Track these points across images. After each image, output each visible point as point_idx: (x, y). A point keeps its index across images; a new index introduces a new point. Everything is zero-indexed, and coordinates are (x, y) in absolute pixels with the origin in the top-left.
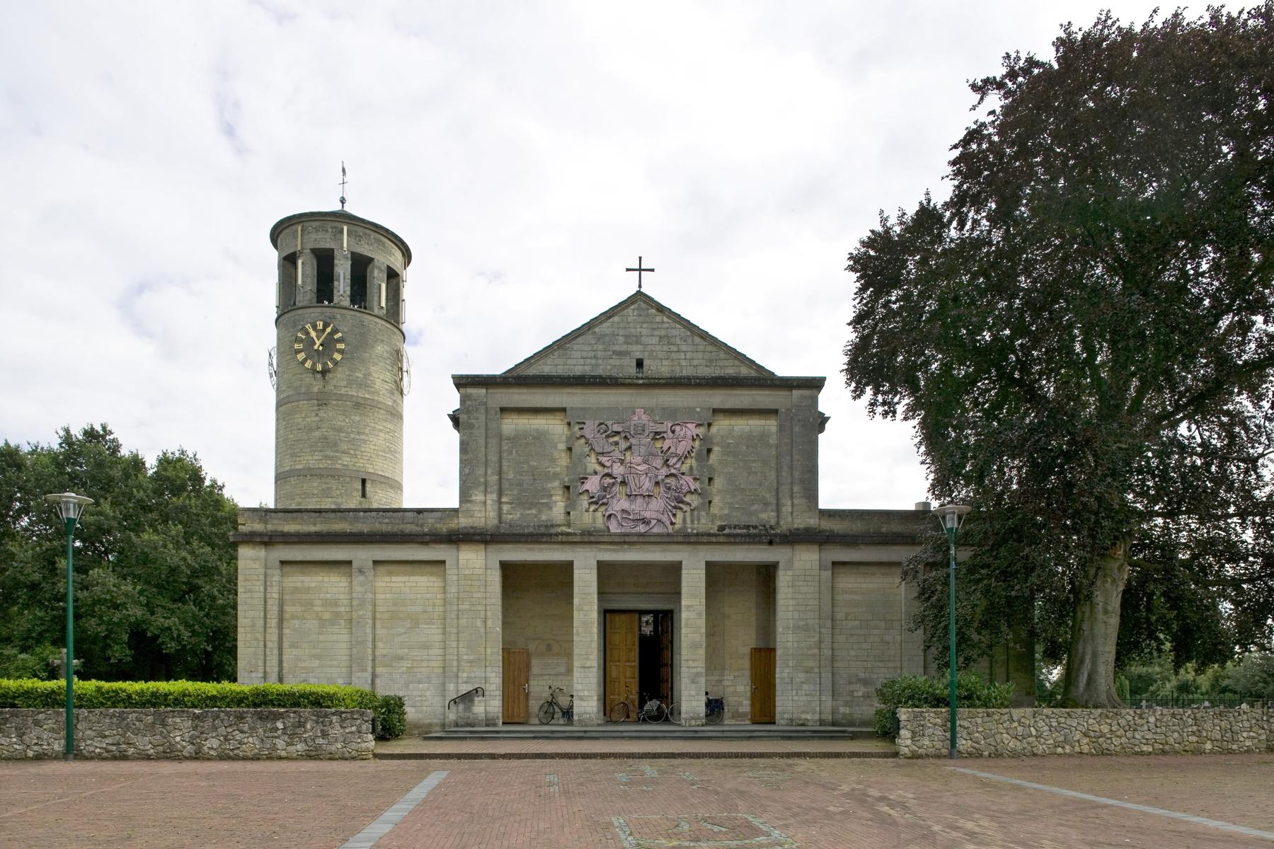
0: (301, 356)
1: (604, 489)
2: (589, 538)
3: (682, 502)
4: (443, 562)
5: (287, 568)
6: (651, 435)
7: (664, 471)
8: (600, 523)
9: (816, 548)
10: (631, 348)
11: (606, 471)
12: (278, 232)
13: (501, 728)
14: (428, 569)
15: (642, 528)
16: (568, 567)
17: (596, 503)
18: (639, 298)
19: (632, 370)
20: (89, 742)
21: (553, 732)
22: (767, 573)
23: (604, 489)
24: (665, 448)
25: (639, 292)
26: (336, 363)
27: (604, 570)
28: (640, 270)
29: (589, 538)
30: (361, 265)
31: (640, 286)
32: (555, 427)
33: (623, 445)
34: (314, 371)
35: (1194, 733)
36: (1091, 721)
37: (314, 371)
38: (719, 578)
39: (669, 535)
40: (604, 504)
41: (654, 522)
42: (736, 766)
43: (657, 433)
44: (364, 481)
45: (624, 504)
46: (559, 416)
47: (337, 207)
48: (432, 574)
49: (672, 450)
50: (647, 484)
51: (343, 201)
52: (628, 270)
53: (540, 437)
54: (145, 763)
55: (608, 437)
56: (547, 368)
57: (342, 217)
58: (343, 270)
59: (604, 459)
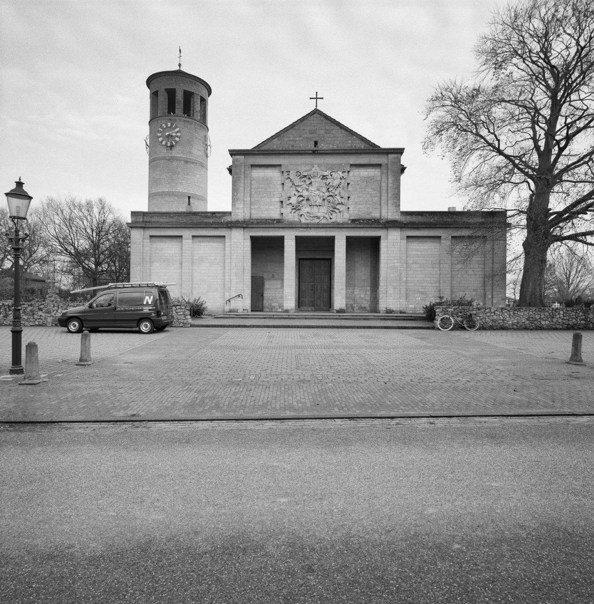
0: (160, 139)
2: (292, 226)
3: (335, 208)
4: (224, 236)
5: (196, 239)
7: (327, 194)
8: (296, 219)
9: (399, 230)
12: (150, 81)
15: (317, 221)
16: (332, 239)
18: (316, 112)
19: (311, 146)
21: (297, 315)
22: (375, 243)
24: (328, 183)
26: (176, 142)
27: (299, 239)
28: (317, 98)
29: (292, 226)
30: (188, 96)
31: (316, 106)
33: (308, 182)
35: (583, 320)
37: (166, 145)
38: (351, 243)
40: (299, 209)
41: (322, 218)
43: (324, 176)
44: (189, 198)
45: (308, 209)
47: (177, 68)
50: (319, 201)
51: (180, 65)
53: (267, 181)
57: (179, 74)
58: (179, 97)
59: (299, 189)
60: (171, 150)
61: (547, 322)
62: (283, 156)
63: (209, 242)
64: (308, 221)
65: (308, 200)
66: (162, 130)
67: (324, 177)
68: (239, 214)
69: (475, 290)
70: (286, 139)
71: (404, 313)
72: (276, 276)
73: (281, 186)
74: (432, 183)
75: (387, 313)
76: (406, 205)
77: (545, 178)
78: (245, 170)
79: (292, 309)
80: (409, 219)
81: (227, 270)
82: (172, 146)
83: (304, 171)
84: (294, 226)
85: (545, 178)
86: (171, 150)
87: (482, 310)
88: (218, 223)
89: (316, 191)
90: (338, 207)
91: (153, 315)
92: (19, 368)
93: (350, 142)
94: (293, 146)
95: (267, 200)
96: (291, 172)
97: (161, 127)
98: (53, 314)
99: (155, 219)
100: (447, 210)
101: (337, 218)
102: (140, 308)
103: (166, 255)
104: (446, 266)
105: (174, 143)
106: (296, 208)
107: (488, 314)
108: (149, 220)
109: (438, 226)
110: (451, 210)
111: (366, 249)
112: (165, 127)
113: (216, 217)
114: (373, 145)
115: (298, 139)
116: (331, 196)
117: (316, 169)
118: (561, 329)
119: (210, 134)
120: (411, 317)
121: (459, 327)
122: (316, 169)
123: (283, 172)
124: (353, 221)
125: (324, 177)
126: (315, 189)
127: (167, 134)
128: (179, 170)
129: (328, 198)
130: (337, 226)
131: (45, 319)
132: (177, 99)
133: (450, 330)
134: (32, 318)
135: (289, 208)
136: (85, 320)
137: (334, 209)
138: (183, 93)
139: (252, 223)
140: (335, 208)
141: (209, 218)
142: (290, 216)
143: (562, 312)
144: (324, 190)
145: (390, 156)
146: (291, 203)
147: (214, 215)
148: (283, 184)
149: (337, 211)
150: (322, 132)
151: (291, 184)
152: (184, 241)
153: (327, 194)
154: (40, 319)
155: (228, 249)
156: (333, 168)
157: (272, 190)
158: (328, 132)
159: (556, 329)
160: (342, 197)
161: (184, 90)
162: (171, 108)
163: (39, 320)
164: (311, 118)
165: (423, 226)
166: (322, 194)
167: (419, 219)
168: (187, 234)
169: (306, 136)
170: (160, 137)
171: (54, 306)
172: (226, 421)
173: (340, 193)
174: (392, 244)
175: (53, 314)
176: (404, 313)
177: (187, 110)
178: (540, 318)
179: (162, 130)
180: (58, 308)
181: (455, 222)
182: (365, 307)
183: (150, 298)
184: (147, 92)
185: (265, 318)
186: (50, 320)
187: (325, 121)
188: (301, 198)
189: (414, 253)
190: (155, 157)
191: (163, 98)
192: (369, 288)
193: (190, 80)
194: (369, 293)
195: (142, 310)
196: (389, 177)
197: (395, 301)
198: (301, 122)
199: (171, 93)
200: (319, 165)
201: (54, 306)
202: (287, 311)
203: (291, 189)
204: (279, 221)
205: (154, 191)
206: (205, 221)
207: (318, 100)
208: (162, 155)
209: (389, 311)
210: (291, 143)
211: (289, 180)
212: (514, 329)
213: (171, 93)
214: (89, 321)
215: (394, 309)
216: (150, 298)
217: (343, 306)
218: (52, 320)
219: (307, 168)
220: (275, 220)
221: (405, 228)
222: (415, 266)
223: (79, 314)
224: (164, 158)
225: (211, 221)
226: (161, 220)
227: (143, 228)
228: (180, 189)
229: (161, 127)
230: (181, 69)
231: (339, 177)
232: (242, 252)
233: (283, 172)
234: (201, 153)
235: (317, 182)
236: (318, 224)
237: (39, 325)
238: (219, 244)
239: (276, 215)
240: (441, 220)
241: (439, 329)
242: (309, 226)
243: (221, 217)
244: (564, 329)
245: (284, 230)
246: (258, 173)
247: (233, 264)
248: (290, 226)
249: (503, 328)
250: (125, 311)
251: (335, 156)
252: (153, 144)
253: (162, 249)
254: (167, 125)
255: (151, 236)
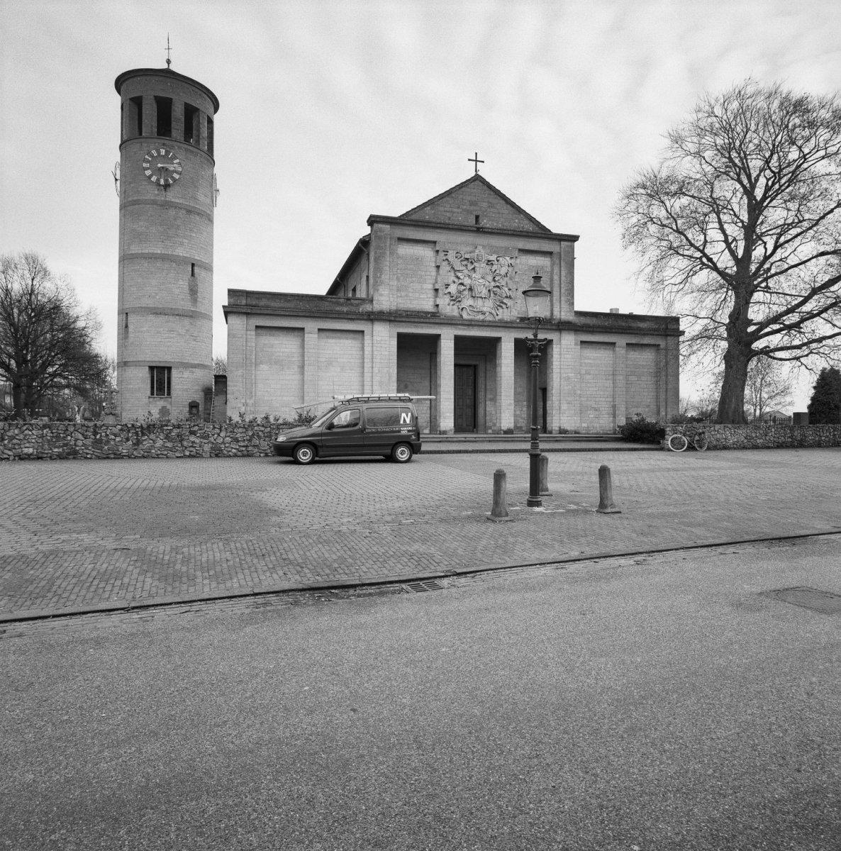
0: (148, 173)
1: (460, 292)
2: (450, 322)
3: (503, 303)
4: (363, 332)
5: (323, 334)
6: (486, 262)
7: (493, 284)
8: (456, 313)
9: (573, 333)
10: (472, 208)
11: (460, 281)
13: (451, 434)
14: (352, 335)
15: (481, 317)
16: (437, 338)
17: (454, 300)
18: (478, 178)
19: (472, 221)
20: (227, 445)
21: (525, 437)
23: (460, 292)
24: (493, 270)
25: (477, 175)
26: (175, 180)
27: (459, 340)
29: (450, 322)
30: (191, 112)
32: (426, 252)
33: (470, 267)
34: (158, 184)
35: (790, 437)
36: (748, 431)
37: (158, 184)
38: (520, 345)
39: (495, 322)
40: (460, 301)
41: (488, 313)
42: (431, 460)
43: (489, 261)
44: (193, 265)
45: (470, 302)
46: (432, 245)
47: (165, 66)
48: (354, 339)
49: (497, 272)
50: (484, 292)
51: (169, 62)
52: (483, 162)
53: (418, 260)
54: (756, 452)
55: (462, 261)
56: (428, 215)
57: (167, 74)
58: (178, 112)
59: (459, 274)
60: (165, 190)
61: (761, 441)
62: (438, 231)
63: (340, 338)
64: (470, 317)
65: (471, 289)
66: (150, 159)
67: (489, 262)
68: (384, 302)
69: (648, 406)
70: (442, 209)
71: (578, 433)
72: (410, 387)
73: (434, 269)
74: (609, 279)
75: (560, 433)
76: (581, 304)
77: (743, 282)
78: (391, 244)
79: (451, 430)
80: (583, 320)
81: (368, 375)
82: (167, 186)
83: (464, 250)
84: (453, 322)
85: (743, 282)
86: (165, 190)
87: (708, 428)
88: (354, 313)
89: (480, 280)
90: (505, 301)
91: (413, 437)
92: (535, 500)
93: (517, 221)
94: (450, 218)
95: (417, 286)
96: (450, 252)
97: (149, 153)
98: (212, 439)
99: (263, 302)
100: (608, 312)
101: (504, 315)
102: (397, 429)
103: (278, 354)
104: (621, 378)
105: (171, 182)
106: (456, 299)
107: (713, 433)
108: (254, 303)
109: (614, 331)
110: (614, 312)
111: (533, 357)
112: (155, 155)
113: (352, 305)
114: (543, 228)
115: (455, 210)
116: (498, 287)
117: (480, 251)
118: (772, 448)
119: (216, 170)
120: (602, 437)
121: (691, 448)
122: (480, 251)
123: (437, 251)
124: (522, 319)
125: (489, 262)
126: (480, 276)
127: (159, 165)
128: (179, 222)
129: (495, 289)
130: (504, 325)
131: (200, 446)
132: (166, 116)
133: (684, 451)
134: (180, 445)
135: (447, 299)
136: (322, 447)
137: (501, 305)
138: (183, 108)
139: (400, 315)
140: (503, 303)
141: (342, 305)
142: (448, 309)
143: (773, 430)
144: (490, 278)
145: (564, 244)
146: (450, 293)
147: (349, 302)
148: (438, 267)
149: (504, 306)
150: (485, 205)
151: (448, 268)
152: (306, 335)
153: (493, 284)
154: (192, 446)
155: (368, 349)
156: (506, 252)
157: (423, 273)
158: (491, 205)
159: (768, 448)
160: (510, 289)
161: (156, 97)
162: (164, 128)
163: (192, 449)
164: (471, 185)
165: (598, 330)
166: (487, 284)
167: (588, 321)
168: (311, 326)
169: (465, 207)
170: (148, 169)
171: (214, 428)
172: (509, 569)
173: (507, 284)
174: (566, 353)
175: (212, 439)
176: (578, 433)
177: (189, 131)
178: (756, 436)
179: (150, 159)
180: (221, 431)
181: (630, 328)
182: (521, 427)
183: (404, 420)
184: (116, 100)
185: (440, 442)
186: (207, 448)
187: (488, 191)
188: (463, 287)
189: (586, 361)
190: (135, 198)
191: (150, 112)
192: (525, 403)
193: (194, 88)
194: (525, 409)
195: (399, 431)
196: (562, 269)
197: (570, 418)
198: (460, 188)
199: (164, 106)
200: (484, 247)
201: (214, 428)
202: (445, 432)
203: (449, 274)
204: (434, 315)
205: (135, 249)
206: (337, 309)
207: (478, 163)
208: (150, 197)
209: (562, 431)
210: (448, 214)
211: (446, 262)
212: (735, 449)
213: (164, 106)
214: (327, 447)
215: (569, 429)
216: (404, 420)
217: (512, 426)
218: (211, 448)
219: (469, 249)
220: (429, 313)
221: (579, 331)
222: (588, 377)
223: (312, 438)
224: (154, 202)
225: (345, 309)
226: (273, 304)
227: (247, 314)
228: (180, 252)
229: (149, 153)
230: (171, 68)
231: (506, 263)
232: (387, 353)
233: (437, 251)
234: (208, 201)
235: (481, 267)
236: (483, 321)
237: (191, 456)
238: (354, 342)
239: (428, 306)
240: (616, 323)
241: (672, 450)
242: (473, 323)
243: (358, 305)
244: (775, 448)
245: (442, 327)
246: (405, 250)
247: (376, 370)
248: (449, 322)
249: (725, 448)
250: (377, 432)
251: (503, 237)
252: (129, 178)
253: (272, 346)
254: (159, 152)
255: (257, 327)
